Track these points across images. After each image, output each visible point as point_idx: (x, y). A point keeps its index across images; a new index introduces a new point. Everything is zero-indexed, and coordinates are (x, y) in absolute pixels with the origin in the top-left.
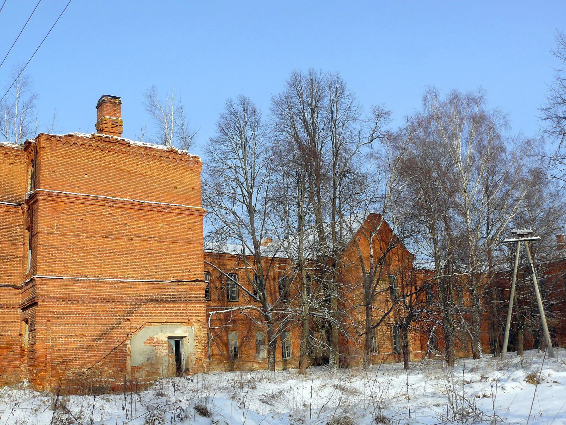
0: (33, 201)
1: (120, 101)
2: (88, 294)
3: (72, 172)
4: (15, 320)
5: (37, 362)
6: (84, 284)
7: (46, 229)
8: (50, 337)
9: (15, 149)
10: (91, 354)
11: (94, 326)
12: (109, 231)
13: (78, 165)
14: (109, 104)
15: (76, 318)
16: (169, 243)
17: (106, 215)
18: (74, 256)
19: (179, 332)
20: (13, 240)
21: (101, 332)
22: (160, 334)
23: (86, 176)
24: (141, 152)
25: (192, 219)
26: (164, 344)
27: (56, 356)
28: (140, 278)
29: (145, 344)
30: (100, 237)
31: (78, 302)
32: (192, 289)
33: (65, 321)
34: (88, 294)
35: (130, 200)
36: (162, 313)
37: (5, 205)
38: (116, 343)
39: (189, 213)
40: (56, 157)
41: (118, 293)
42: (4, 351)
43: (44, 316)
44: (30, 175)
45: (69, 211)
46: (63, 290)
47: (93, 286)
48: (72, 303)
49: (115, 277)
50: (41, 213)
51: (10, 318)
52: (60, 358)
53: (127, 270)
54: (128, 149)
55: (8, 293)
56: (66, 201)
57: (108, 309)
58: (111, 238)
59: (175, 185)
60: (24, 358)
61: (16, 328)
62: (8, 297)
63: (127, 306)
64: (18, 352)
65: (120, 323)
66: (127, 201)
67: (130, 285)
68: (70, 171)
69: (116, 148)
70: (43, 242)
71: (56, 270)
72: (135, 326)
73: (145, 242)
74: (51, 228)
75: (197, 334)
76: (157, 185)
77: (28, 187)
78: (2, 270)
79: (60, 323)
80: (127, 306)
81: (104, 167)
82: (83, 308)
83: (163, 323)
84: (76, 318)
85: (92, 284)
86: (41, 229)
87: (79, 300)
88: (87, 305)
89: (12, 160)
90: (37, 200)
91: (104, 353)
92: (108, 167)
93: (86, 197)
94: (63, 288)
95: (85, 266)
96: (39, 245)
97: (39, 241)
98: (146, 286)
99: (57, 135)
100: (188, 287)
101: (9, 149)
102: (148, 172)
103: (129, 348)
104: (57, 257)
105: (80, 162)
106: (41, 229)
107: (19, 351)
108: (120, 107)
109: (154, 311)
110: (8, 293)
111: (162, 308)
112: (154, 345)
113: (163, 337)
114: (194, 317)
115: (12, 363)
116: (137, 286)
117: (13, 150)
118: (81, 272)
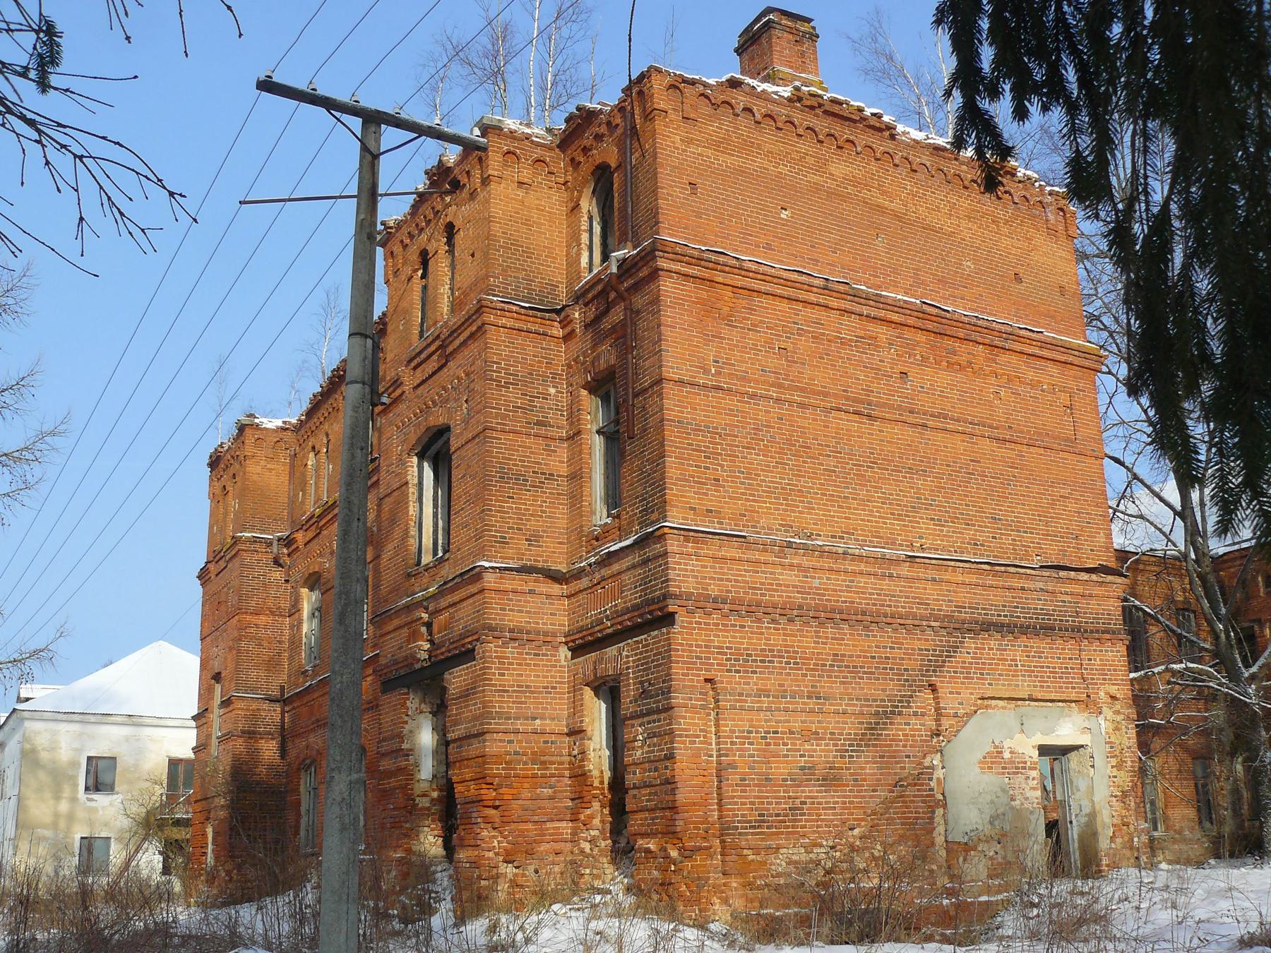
0: (631, 281)
1: (814, 28)
2: (818, 594)
3: (744, 195)
4: (552, 682)
5: (681, 823)
6: (806, 562)
7: (687, 370)
8: (714, 737)
9: (532, 141)
10: (834, 798)
11: (841, 705)
12: (860, 394)
13: (759, 176)
14: (786, 34)
15: (789, 674)
16: (1019, 447)
17: (850, 340)
18: (769, 466)
19: (1067, 730)
20: (539, 423)
21: (859, 723)
22: (1018, 736)
23: (785, 214)
24: (924, 162)
25: (1071, 379)
26: (1031, 769)
27: (736, 803)
28: (956, 552)
29: (982, 768)
30: (839, 410)
31: (791, 620)
32: (1090, 595)
33: (756, 685)
34: (818, 594)
35: (913, 300)
36: (1020, 667)
37: (514, 308)
38: (904, 762)
39: (1063, 358)
40: (698, 145)
41: (898, 596)
42: (526, 785)
43: (695, 663)
44: (586, 218)
45: (748, 319)
46: (745, 576)
47: (831, 570)
48: (774, 621)
49: (887, 543)
50: (669, 317)
51: (538, 676)
52: (748, 809)
53: (918, 523)
54: (890, 148)
55: (531, 592)
56: (739, 284)
57: (877, 646)
58: (869, 416)
59: (1016, 270)
60: (588, 812)
61: (555, 709)
62: (531, 607)
63: (927, 640)
64: (566, 791)
65: (911, 696)
66: (905, 302)
67: (931, 574)
68: (740, 194)
69: (863, 138)
70: (679, 411)
71: (722, 507)
72: (952, 708)
73: (958, 437)
74: (701, 368)
75: (1112, 740)
76: (972, 266)
77: (580, 254)
78: (509, 518)
79: (743, 689)
80: (927, 640)
81: (831, 194)
82: (806, 640)
83: (1019, 703)
84: (789, 674)
85: (827, 563)
86: (672, 368)
87: (795, 612)
88: (815, 632)
89: (526, 174)
90: (654, 274)
91: (871, 797)
92: (840, 195)
93: (795, 276)
94: (746, 571)
95: (803, 501)
96: (668, 420)
97: (668, 409)
98: (973, 579)
99: (697, 77)
100: (1078, 589)
101: (515, 138)
102: (948, 225)
103: (938, 779)
104: (722, 466)
105: (765, 169)
106: (672, 368)
107: (566, 785)
108: (815, 47)
109: (998, 659)
110: (531, 592)
111: (1017, 650)
112: (1003, 773)
113: (1026, 746)
114: (1101, 684)
115: (549, 825)
116: (946, 577)
117: (526, 142)
118: (794, 521)
